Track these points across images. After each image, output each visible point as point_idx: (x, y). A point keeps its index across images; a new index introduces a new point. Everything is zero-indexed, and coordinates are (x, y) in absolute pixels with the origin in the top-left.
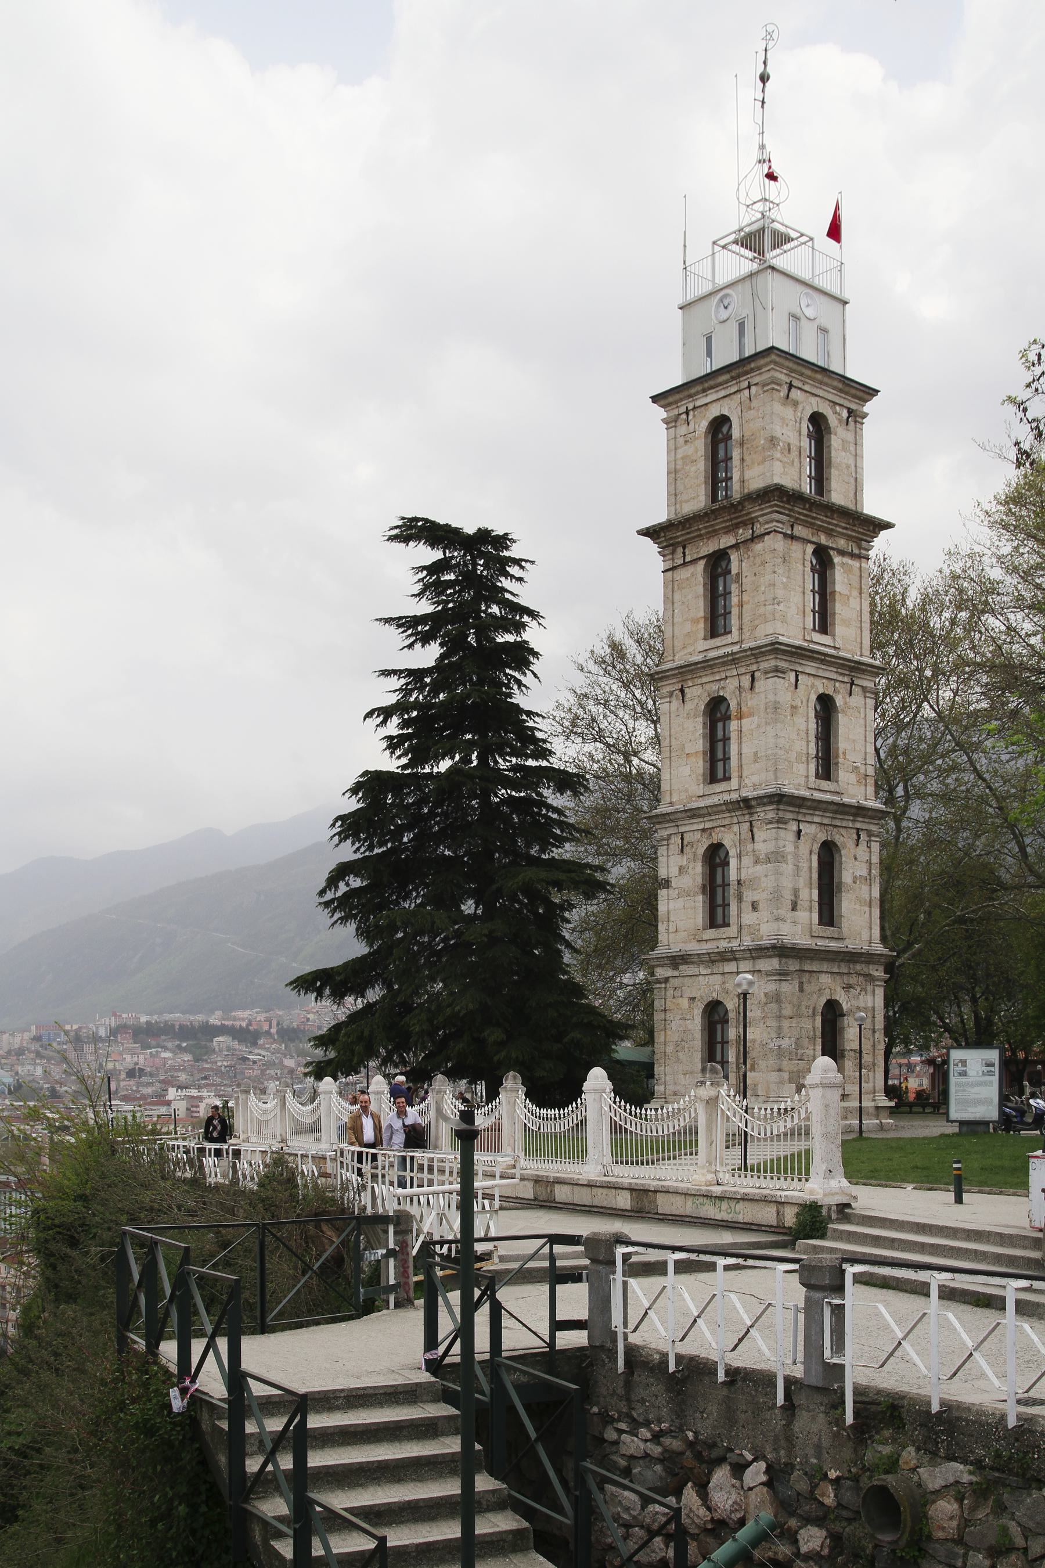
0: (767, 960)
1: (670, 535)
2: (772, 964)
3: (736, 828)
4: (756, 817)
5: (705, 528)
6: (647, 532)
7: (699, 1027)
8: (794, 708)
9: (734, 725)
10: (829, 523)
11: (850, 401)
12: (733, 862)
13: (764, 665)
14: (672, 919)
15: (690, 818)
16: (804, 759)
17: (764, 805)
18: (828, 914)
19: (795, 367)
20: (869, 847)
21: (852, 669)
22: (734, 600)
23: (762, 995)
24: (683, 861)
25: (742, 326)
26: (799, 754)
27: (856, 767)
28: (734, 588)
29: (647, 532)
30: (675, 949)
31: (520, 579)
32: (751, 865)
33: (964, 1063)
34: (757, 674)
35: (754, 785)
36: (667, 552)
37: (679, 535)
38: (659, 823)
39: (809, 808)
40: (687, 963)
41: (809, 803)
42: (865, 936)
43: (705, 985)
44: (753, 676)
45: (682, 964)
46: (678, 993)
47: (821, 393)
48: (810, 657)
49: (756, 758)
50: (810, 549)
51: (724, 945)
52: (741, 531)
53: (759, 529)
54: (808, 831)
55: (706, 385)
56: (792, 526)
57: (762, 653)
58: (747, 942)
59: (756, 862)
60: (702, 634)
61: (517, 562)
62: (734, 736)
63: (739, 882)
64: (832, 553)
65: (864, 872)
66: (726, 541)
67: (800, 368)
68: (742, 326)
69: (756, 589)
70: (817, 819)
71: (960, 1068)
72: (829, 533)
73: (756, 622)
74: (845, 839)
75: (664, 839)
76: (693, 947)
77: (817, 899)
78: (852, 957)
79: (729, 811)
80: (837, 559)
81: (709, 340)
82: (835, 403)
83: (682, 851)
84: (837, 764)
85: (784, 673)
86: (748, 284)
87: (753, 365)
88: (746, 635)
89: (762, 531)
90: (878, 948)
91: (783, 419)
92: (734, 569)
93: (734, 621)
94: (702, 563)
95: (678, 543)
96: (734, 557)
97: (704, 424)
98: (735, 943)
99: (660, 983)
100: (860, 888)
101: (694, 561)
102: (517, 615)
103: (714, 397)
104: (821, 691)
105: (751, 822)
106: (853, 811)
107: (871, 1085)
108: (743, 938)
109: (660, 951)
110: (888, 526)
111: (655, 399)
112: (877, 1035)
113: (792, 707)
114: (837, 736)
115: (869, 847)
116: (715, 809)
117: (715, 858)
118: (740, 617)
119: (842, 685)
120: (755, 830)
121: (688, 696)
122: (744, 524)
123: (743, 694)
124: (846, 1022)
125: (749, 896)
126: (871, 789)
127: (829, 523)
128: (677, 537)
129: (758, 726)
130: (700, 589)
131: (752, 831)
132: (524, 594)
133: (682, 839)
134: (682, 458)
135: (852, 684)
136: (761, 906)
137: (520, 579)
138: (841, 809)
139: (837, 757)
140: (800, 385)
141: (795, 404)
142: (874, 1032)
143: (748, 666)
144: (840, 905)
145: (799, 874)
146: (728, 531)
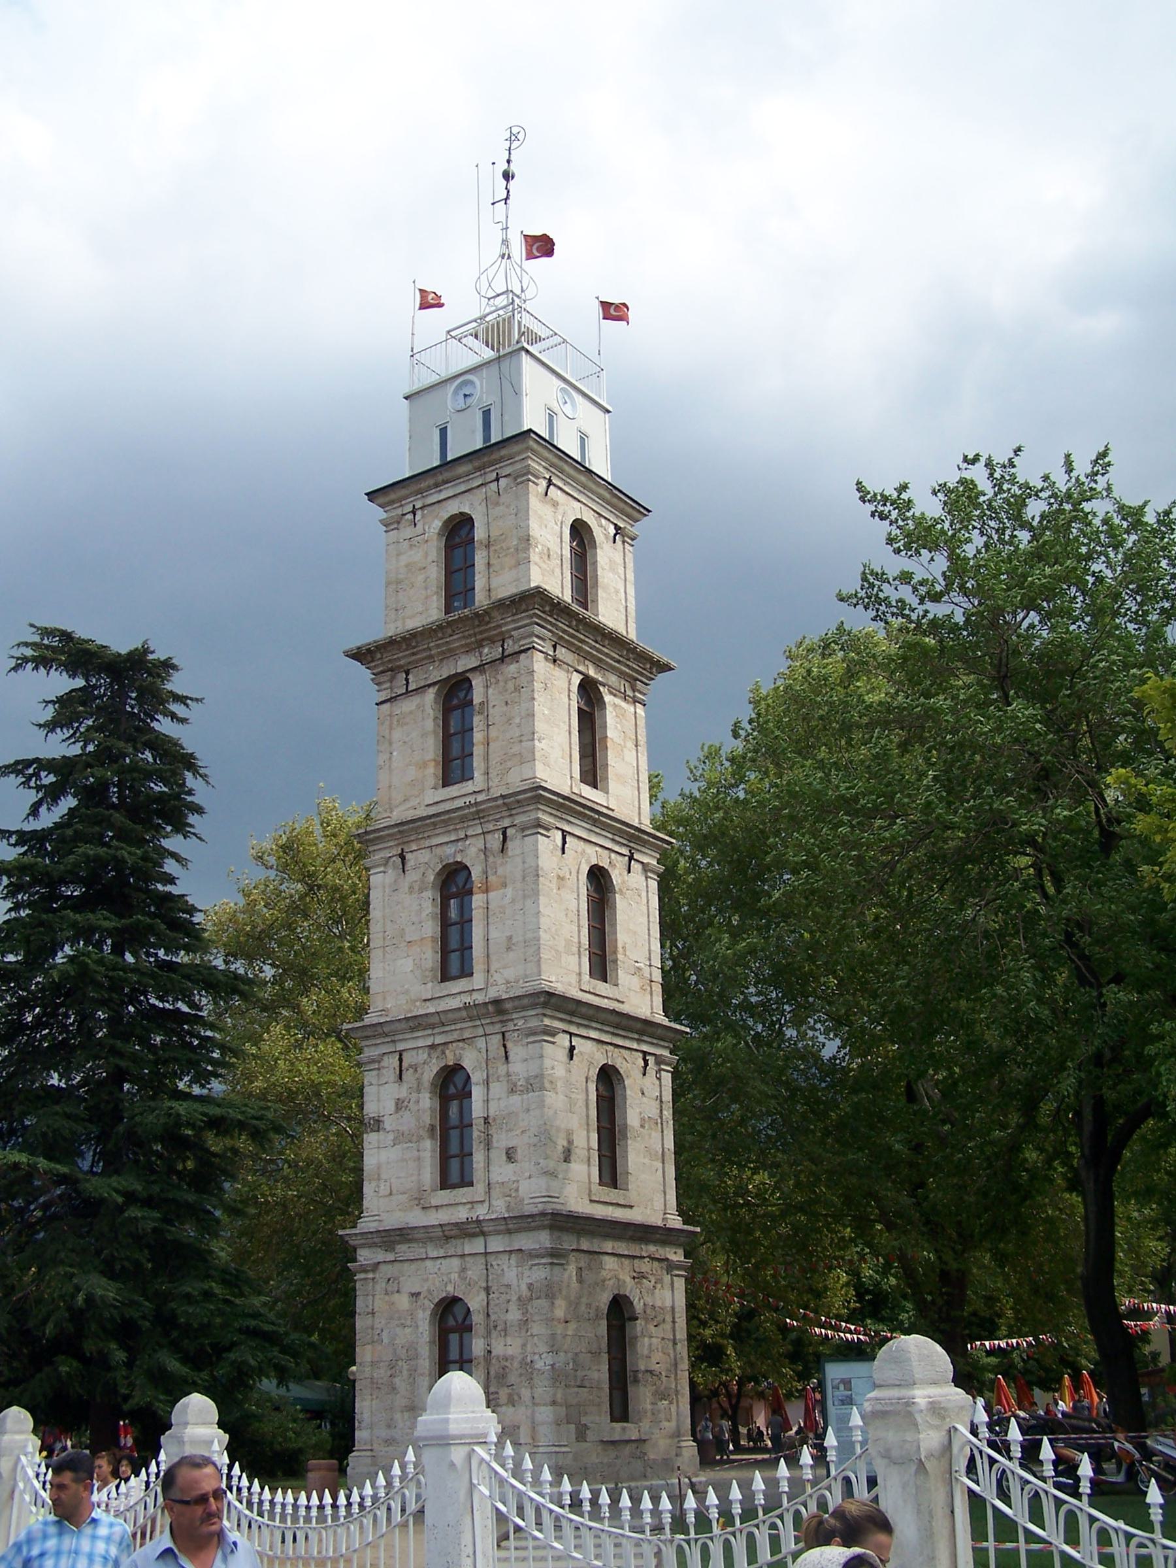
0: (531, 1234)
1: (387, 657)
2: (543, 1239)
3: (481, 1043)
4: (511, 1026)
5: (438, 646)
6: (361, 655)
7: (426, 1337)
8: (561, 878)
9: (477, 900)
10: (598, 650)
11: (617, 516)
12: (477, 1093)
13: (519, 820)
14: (384, 1176)
15: (412, 1030)
16: (575, 949)
17: (524, 1008)
18: (611, 1170)
19: (555, 460)
20: (659, 1079)
21: (631, 838)
22: (478, 736)
23: (524, 1287)
24: (403, 1092)
25: (487, 414)
26: (568, 943)
27: (639, 969)
28: (477, 721)
29: (361, 655)
30: (393, 1220)
31: (183, 721)
32: (504, 1095)
33: (847, 1383)
34: (510, 832)
35: (508, 982)
36: (383, 678)
37: (402, 657)
38: (367, 1038)
39: (583, 1017)
40: (410, 1241)
41: (584, 1010)
42: (659, 1205)
43: (440, 1274)
44: (504, 834)
45: (399, 1243)
46: (392, 1287)
48: (580, 813)
49: (510, 946)
50: (577, 679)
51: (462, 1214)
52: (486, 650)
53: (510, 646)
54: (582, 1049)
55: (440, 478)
56: (555, 647)
57: (518, 802)
58: (500, 1207)
59: (512, 1091)
60: (431, 781)
61: (182, 699)
62: (477, 915)
63: (486, 1120)
64: (601, 688)
65: (654, 1112)
67: (561, 464)
68: (487, 414)
69: (509, 721)
70: (594, 1034)
71: (842, 1392)
72: (598, 664)
73: (509, 764)
74: (629, 1065)
75: (373, 1061)
76: (417, 1218)
77: (596, 1148)
78: (643, 1233)
79: (471, 1019)
81: (443, 432)
83: (401, 1078)
84: (615, 961)
85: (548, 830)
86: (494, 368)
87: (503, 452)
88: (494, 782)
89: (517, 649)
90: (676, 1222)
91: (540, 517)
92: (477, 698)
93: (477, 762)
94: (431, 693)
95: (402, 666)
96: (477, 682)
97: (437, 524)
98: (481, 1212)
99: (366, 1271)
100: (650, 1135)
101: (420, 690)
102: (178, 760)
104: (594, 862)
105: (503, 1034)
106: (639, 1026)
107: (673, 1424)
108: (494, 1202)
109: (366, 1224)
110: (665, 668)
111: (372, 495)
112: (679, 1347)
113: (559, 877)
114: (614, 925)
115: (659, 1079)
116: (450, 1016)
117: (452, 1085)
118: (487, 758)
119: (620, 858)
120: (509, 1045)
121: (410, 864)
123: (491, 859)
124: (639, 1329)
125: (501, 1140)
126: (658, 1000)
127: (598, 650)
128: (399, 659)
129: (513, 901)
130: (429, 724)
131: (505, 1046)
133: (401, 1060)
134: (406, 566)
135: (631, 858)
136: (519, 1155)
137: (183, 721)
138: (625, 1022)
139: (615, 952)
140: (560, 484)
141: (555, 504)
142: (675, 1344)
143: (497, 820)
144: (625, 1157)
145: (570, 1106)
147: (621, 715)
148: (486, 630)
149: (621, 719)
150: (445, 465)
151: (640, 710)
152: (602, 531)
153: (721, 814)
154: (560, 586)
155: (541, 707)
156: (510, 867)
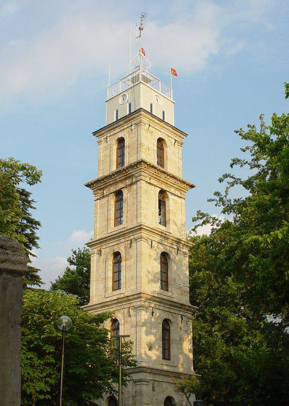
6: (88, 186)
25: (130, 105)
29: (88, 186)
47: (162, 131)
56: (150, 179)
64: (168, 193)
66: (120, 186)
80: (170, 196)
82: (181, 190)
101: (108, 195)
103: (118, 131)
122: (129, 177)
132: (34, 214)
141: (152, 133)
146: (121, 181)
147: (176, 202)
148: (127, 175)
149: (173, 203)
150: (118, 121)
151: (183, 201)
152: (169, 142)
153: (260, 266)
154: (153, 159)
155: (144, 198)
156: (133, 252)
